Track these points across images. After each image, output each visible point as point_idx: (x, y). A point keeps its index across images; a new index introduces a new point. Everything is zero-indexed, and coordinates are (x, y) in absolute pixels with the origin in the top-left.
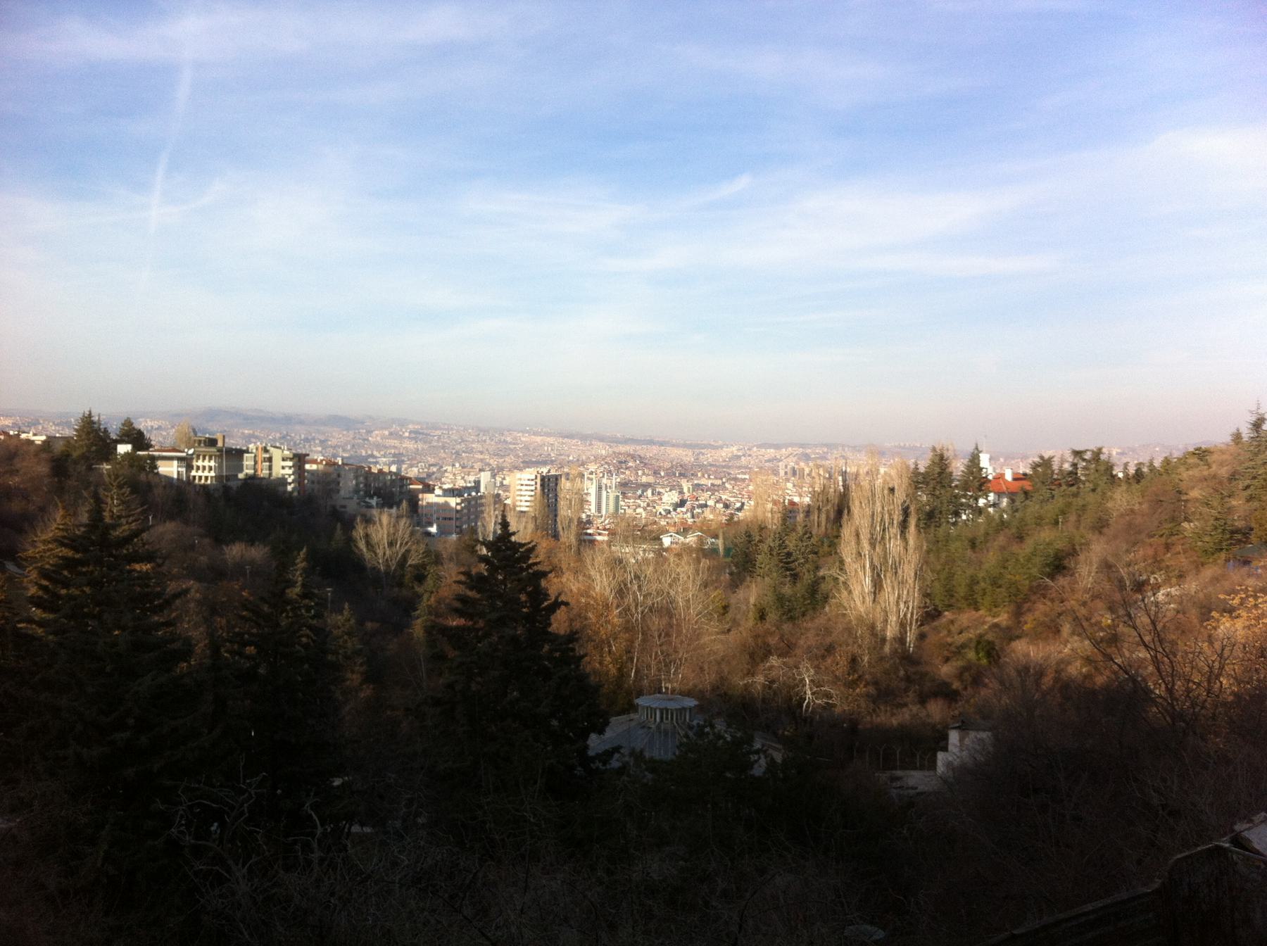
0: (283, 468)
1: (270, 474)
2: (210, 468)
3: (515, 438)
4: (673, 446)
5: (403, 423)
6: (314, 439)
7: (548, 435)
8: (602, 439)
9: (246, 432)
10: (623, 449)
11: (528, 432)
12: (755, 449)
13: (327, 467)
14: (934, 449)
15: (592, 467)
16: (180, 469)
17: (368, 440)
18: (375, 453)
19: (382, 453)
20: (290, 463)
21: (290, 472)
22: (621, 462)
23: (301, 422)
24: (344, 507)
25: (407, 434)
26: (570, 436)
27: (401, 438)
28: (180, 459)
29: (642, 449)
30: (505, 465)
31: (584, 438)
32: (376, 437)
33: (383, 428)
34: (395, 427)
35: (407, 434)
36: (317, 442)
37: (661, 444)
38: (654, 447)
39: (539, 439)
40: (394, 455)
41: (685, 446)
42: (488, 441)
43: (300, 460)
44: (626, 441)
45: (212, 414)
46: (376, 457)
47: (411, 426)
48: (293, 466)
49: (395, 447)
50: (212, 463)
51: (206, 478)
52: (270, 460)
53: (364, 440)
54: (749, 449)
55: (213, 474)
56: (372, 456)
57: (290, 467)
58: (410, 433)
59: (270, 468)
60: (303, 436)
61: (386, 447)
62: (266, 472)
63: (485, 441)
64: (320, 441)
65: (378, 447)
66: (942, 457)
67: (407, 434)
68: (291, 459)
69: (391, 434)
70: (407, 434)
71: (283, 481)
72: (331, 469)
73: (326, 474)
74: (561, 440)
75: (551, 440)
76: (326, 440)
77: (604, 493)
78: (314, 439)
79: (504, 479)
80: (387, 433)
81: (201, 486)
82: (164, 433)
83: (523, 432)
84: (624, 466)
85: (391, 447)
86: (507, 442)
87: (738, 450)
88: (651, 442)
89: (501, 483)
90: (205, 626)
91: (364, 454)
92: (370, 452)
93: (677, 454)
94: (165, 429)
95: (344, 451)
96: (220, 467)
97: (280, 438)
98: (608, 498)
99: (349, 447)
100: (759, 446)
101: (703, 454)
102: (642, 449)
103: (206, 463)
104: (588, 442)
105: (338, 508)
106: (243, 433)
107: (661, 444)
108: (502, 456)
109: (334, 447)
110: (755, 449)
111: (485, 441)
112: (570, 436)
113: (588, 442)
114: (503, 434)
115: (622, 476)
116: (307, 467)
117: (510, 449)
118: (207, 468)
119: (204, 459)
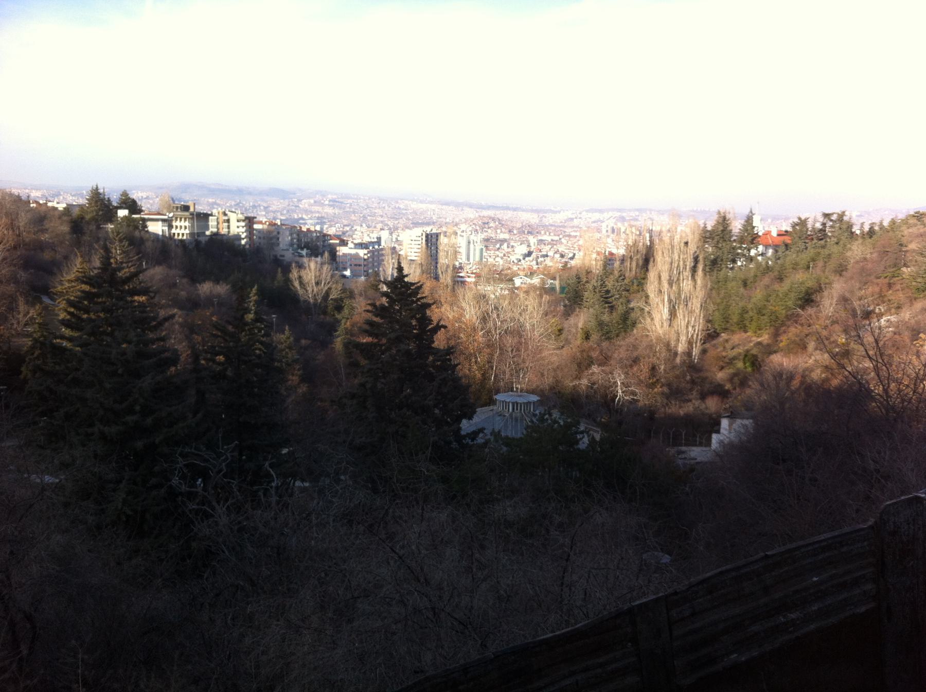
0: (238, 227)
1: (229, 232)
4: (523, 211)
5: (324, 194)
6: (259, 206)
7: (431, 203)
10: (486, 213)
12: (584, 213)
16: (164, 228)
17: (298, 206)
18: (304, 216)
19: (309, 216)
20: (243, 224)
21: (244, 230)
22: (484, 223)
23: (250, 194)
24: (283, 256)
27: (323, 205)
28: (163, 221)
30: (399, 225)
31: (458, 205)
32: (304, 204)
33: (309, 198)
34: (318, 197)
36: (262, 208)
37: (515, 209)
40: (318, 218)
41: (533, 211)
42: (387, 207)
43: (250, 221)
44: (489, 207)
45: (186, 187)
47: (330, 197)
51: (183, 235)
52: (228, 221)
53: (296, 206)
56: (302, 219)
57: (243, 227)
58: (330, 201)
59: (229, 227)
60: (251, 204)
61: (312, 212)
63: (384, 208)
64: (264, 207)
65: (306, 212)
66: (724, 218)
68: (244, 221)
69: (315, 202)
70: (327, 202)
71: (238, 238)
73: (269, 232)
76: (267, 207)
77: (472, 245)
78: (259, 206)
80: (312, 201)
82: (151, 202)
84: (486, 226)
85: (315, 212)
86: (399, 208)
88: (508, 208)
89: (397, 239)
92: (300, 216)
94: (152, 199)
97: (235, 205)
98: (475, 250)
99: (285, 212)
100: (587, 211)
101: (545, 217)
104: (460, 209)
106: (208, 202)
107: (515, 209)
108: (397, 219)
109: (274, 212)
111: (384, 208)
114: (397, 202)
118: (183, 228)
119: (181, 220)
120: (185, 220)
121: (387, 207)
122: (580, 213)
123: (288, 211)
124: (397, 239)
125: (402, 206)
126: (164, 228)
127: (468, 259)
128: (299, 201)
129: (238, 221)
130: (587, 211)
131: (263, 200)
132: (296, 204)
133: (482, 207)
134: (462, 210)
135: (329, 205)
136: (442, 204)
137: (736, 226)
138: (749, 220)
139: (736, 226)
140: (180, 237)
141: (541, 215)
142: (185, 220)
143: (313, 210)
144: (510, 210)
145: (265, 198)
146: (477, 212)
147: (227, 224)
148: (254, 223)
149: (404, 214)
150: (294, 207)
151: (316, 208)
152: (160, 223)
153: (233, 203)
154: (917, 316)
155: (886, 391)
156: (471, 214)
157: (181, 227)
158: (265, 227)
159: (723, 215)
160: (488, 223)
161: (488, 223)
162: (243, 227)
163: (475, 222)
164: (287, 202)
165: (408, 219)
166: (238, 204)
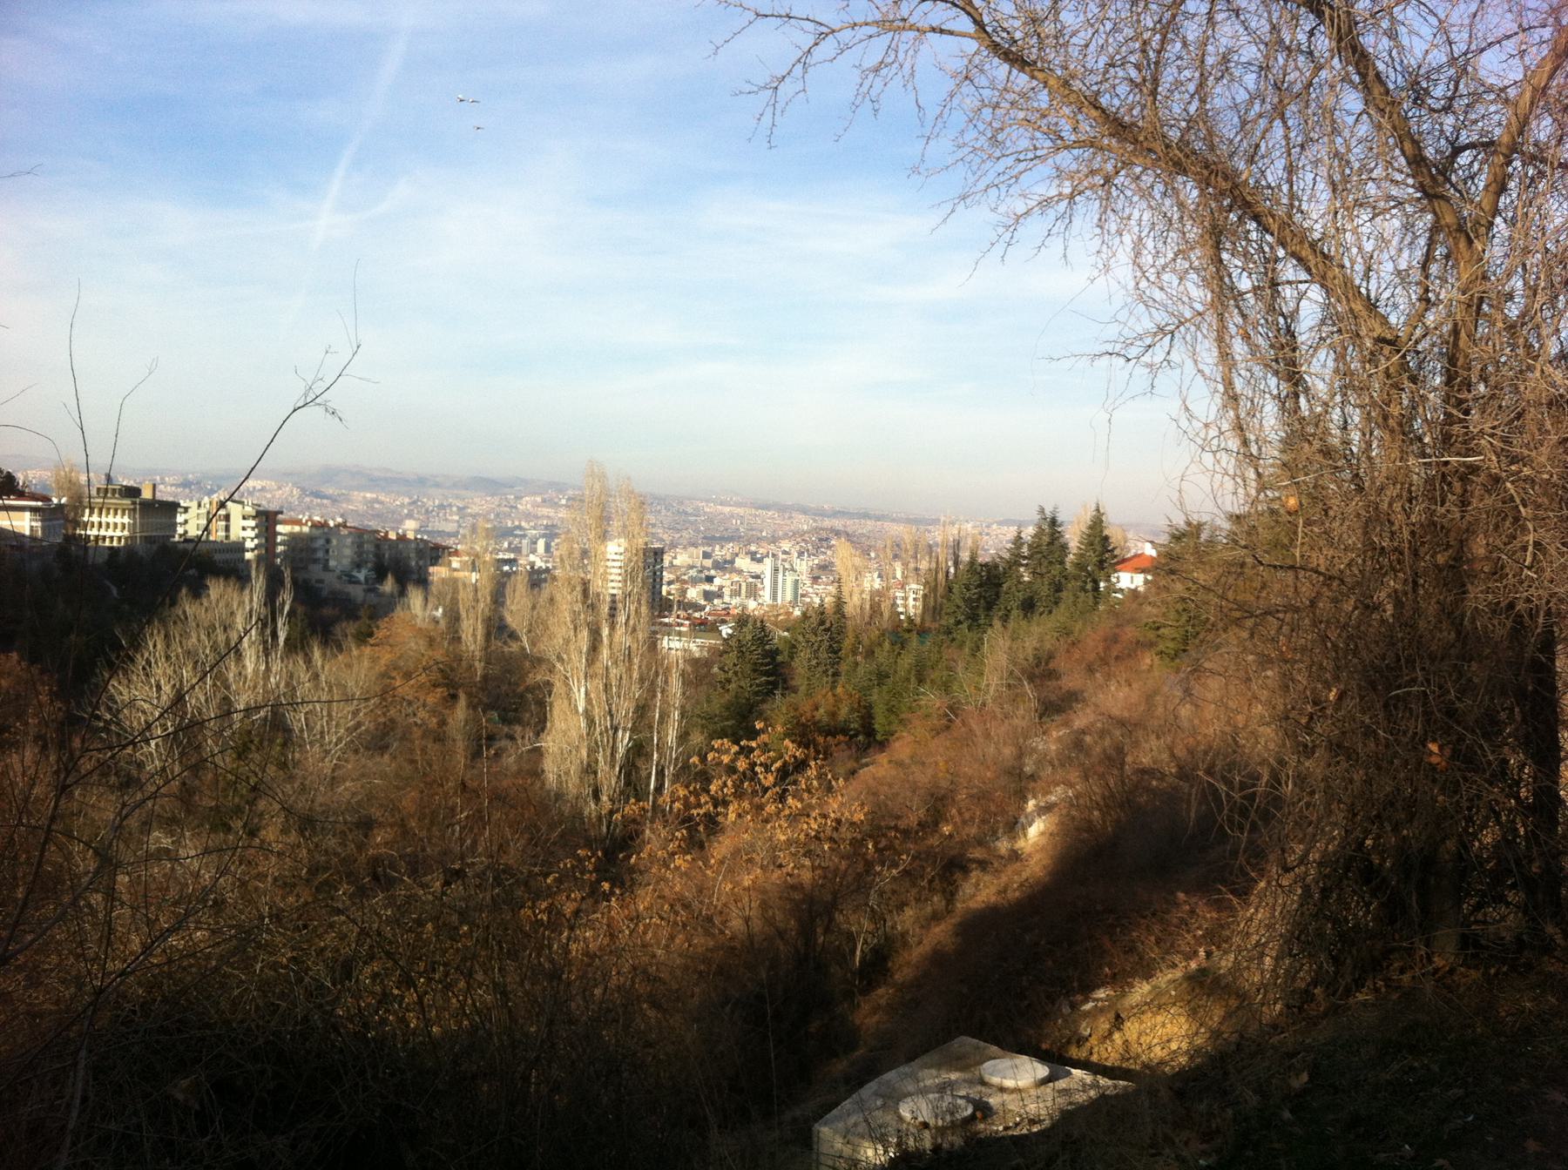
0: (244, 529)
1: (227, 537)
2: (123, 526)
3: (697, 509)
4: (893, 520)
5: (560, 488)
6: (450, 505)
7: (738, 505)
8: (804, 511)
9: (368, 495)
10: (827, 523)
11: (714, 501)
12: (995, 526)
13: (314, 530)
14: (1042, 511)
15: (786, 545)
16: (34, 524)
17: (516, 507)
18: (523, 524)
19: (532, 524)
20: (252, 523)
21: (253, 534)
22: (821, 540)
23: (437, 485)
24: (321, 581)
25: (564, 502)
26: (767, 507)
27: (555, 505)
28: (33, 510)
29: (854, 524)
30: (681, 541)
31: (782, 509)
32: (526, 504)
33: (534, 494)
34: (551, 493)
35: (564, 502)
36: (455, 509)
37: (878, 518)
38: (869, 522)
39: (727, 510)
40: (547, 527)
41: (908, 521)
42: (664, 511)
43: (267, 520)
44: (836, 514)
45: (329, 474)
46: (525, 529)
47: (570, 492)
48: (257, 526)
49: (548, 517)
50: (126, 520)
51: (120, 538)
52: (227, 518)
53: (512, 507)
54: (988, 527)
55: (126, 533)
56: (520, 528)
57: (253, 529)
58: (568, 500)
59: (227, 529)
60: (437, 502)
61: (537, 517)
62: (222, 534)
63: (659, 511)
64: (458, 507)
65: (528, 516)
66: (1054, 522)
67: (564, 502)
68: (254, 518)
69: (544, 501)
70: (564, 502)
71: (239, 547)
72: (317, 532)
73: (310, 538)
74: (753, 511)
75: (740, 511)
76: (464, 508)
77: (780, 576)
78: (450, 505)
79: (675, 558)
80: (539, 499)
81: (111, 548)
82: (269, 496)
83: (708, 501)
84: (825, 544)
85: (543, 517)
86: (686, 513)
87: (974, 527)
88: (866, 516)
89: (671, 563)
90: (1186, 724)
91: (509, 524)
92: (517, 523)
93: (897, 530)
94: (270, 491)
95: (488, 521)
96: (133, 527)
97: (410, 504)
98: (784, 580)
99: (492, 516)
100: (1000, 523)
101: (929, 532)
102: (854, 524)
103: (118, 519)
104: (787, 515)
105: (313, 582)
106: (364, 497)
107: (878, 518)
108: (678, 531)
109: (474, 516)
110: (995, 526)
111: (659, 511)
112: (767, 507)
113: (787, 515)
114: (682, 503)
115: (822, 557)
116: (280, 528)
117: (690, 522)
118: (119, 526)
119: (116, 514)
120: (123, 514)
121: (664, 511)
122: (988, 527)
123: (497, 515)
124: (671, 563)
125: (690, 510)
126: (34, 524)
127: (774, 597)
128: (518, 498)
129: (244, 518)
130: (1000, 523)
131: (457, 497)
132: (512, 503)
133: (822, 513)
134: (790, 518)
135: (567, 506)
136: (757, 508)
137: (1073, 538)
138: (1097, 523)
139: (1073, 538)
140: (107, 543)
141: (922, 528)
142: (123, 514)
143: (540, 514)
144: (870, 518)
145: (463, 492)
146: (815, 521)
147: (224, 523)
148: (276, 523)
149: (691, 523)
150: (507, 509)
151: (545, 511)
152: (27, 515)
153: (407, 500)
154: (882, 784)
155: (1380, 865)
156: (804, 523)
157: (108, 525)
158: (306, 529)
159: (1048, 514)
160: (827, 539)
161: (827, 539)
162: (253, 529)
163: (806, 537)
164: (496, 500)
165: (697, 531)
166: (414, 503)
